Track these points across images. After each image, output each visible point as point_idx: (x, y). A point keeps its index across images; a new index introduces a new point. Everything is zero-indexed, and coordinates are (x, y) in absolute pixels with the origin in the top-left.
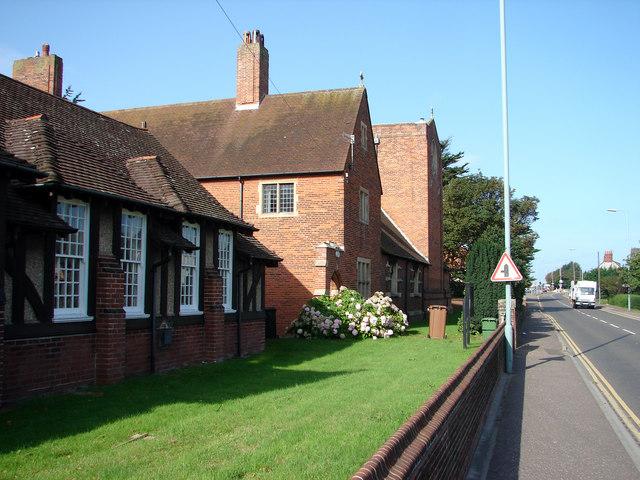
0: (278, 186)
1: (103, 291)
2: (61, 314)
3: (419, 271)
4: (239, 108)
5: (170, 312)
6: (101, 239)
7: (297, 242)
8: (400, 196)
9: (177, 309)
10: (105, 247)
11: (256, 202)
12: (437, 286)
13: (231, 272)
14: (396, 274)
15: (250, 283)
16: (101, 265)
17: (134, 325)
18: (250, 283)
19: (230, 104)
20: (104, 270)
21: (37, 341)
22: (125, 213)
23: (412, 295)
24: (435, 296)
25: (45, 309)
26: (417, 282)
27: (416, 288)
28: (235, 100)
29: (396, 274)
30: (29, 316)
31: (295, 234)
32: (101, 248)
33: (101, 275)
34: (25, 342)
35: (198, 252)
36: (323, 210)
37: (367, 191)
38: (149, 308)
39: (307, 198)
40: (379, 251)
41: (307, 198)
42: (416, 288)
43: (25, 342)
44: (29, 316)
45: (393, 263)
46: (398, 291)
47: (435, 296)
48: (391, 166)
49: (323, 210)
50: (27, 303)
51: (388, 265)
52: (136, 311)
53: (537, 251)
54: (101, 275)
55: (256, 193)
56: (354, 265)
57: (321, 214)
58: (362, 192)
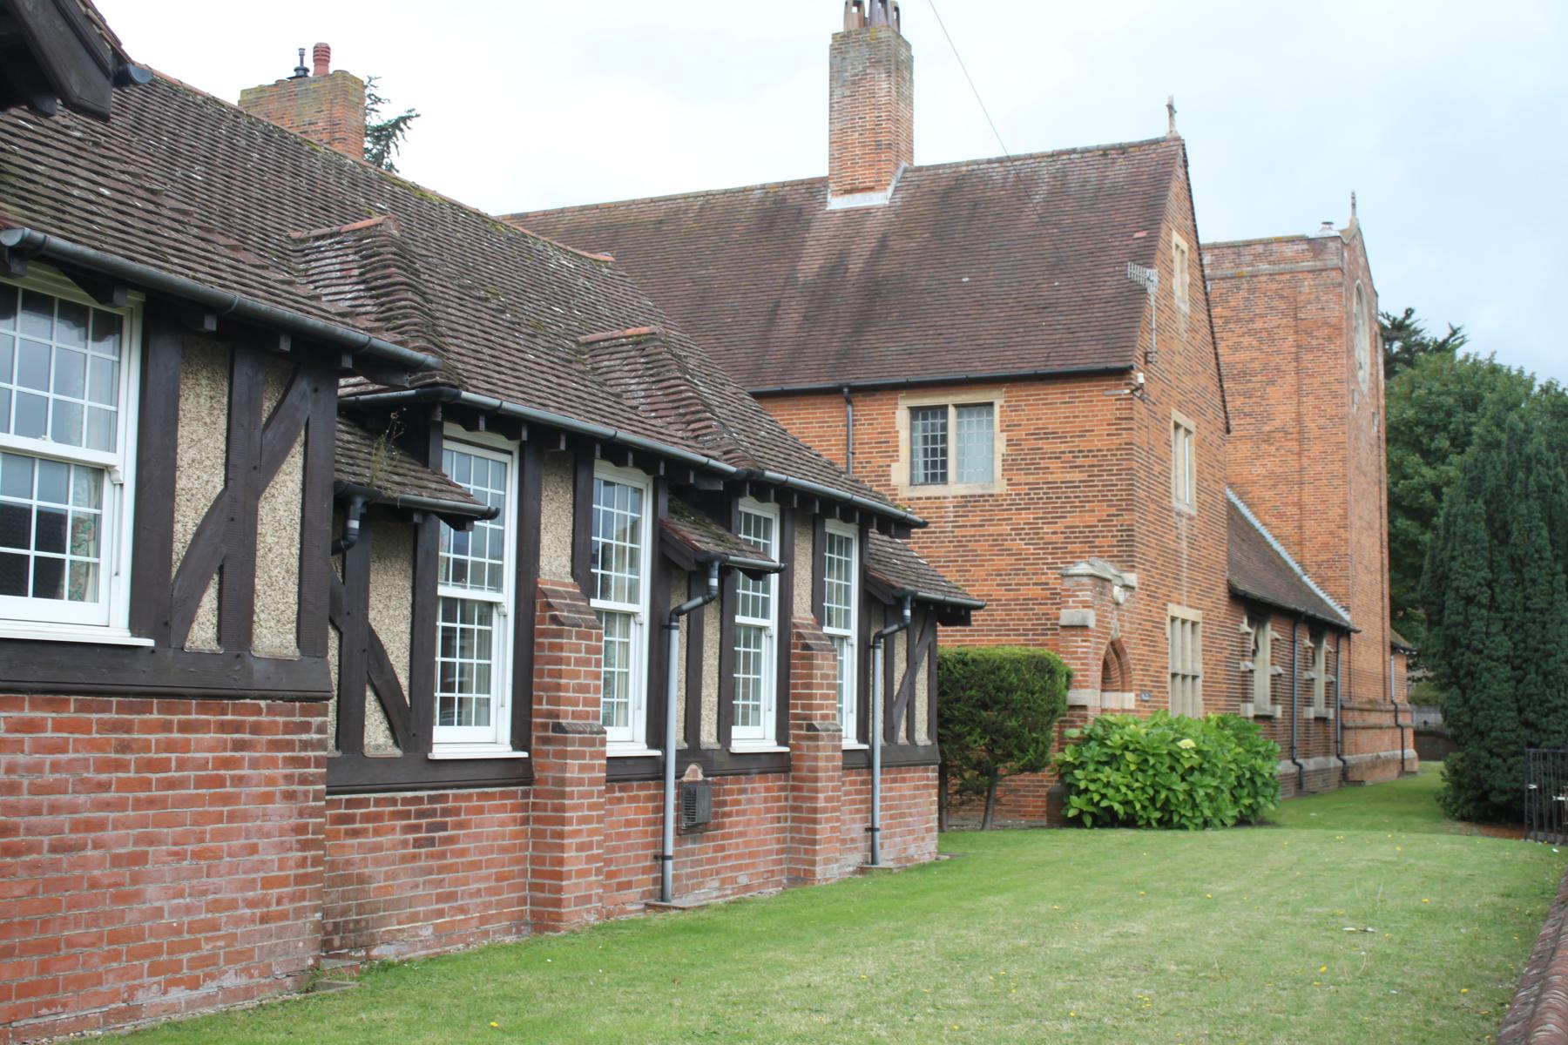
0: (952, 411)
1: (552, 674)
2: (449, 742)
3: (1326, 646)
4: (837, 203)
5: (708, 735)
6: (546, 539)
7: (1004, 562)
8: (1268, 439)
9: (724, 735)
10: (555, 562)
11: (892, 454)
12: (1375, 692)
13: (645, 617)
14: (1265, 653)
15: (900, 667)
16: (800, 636)
17: (622, 771)
18: (900, 667)
19: (813, 189)
20: (555, 619)
21: (394, 802)
22: (603, 471)
23: (1311, 713)
24: (1373, 719)
25: (410, 726)
26: (1320, 675)
27: (1319, 692)
28: (823, 182)
29: (1265, 653)
30: (376, 734)
31: (997, 540)
32: (544, 562)
33: (544, 633)
34: (444, 798)
35: (774, 579)
36: (1077, 476)
37: (1189, 423)
38: (657, 734)
39: (1033, 444)
40: (1221, 592)
41: (1033, 444)
42: (1319, 692)
43: (444, 798)
44: (376, 734)
45: (1317, 636)
46: (1274, 700)
47: (1373, 719)
48: (1241, 356)
49: (1077, 476)
50: (370, 696)
51: (1245, 627)
52: (627, 738)
53: (1409, 313)
54: (544, 633)
55: (891, 431)
56: (1159, 625)
57: (1070, 484)
58: (1177, 426)
